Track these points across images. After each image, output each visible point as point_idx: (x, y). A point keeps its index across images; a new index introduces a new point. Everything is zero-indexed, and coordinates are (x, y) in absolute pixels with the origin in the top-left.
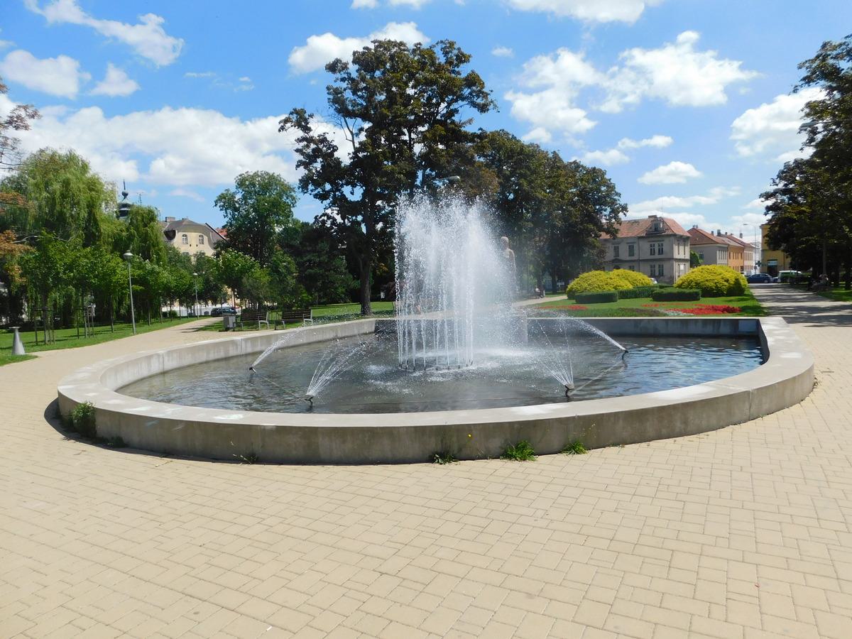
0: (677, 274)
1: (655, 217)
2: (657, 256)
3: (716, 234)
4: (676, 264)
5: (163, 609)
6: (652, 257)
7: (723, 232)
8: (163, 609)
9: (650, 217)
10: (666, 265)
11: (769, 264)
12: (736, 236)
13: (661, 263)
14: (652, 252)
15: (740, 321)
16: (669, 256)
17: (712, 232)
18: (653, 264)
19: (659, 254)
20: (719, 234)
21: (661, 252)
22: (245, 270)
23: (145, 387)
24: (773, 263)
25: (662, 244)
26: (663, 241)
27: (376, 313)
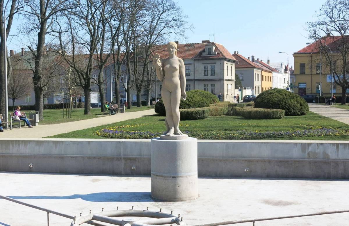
0: (226, 93)
1: (208, 42)
2: (210, 77)
3: (251, 60)
4: (225, 83)
5: (79, 225)
6: (206, 77)
7: (256, 59)
8: (79, 225)
9: (203, 42)
10: (217, 85)
11: (300, 87)
12: (265, 62)
13: (213, 83)
14: (206, 73)
15: (9, 105)
16: (219, 77)
17: (249, 58)
18: (206, 83)
19: (212, 75)
20: (253, 60)
21: (213, 74)
22: (22, 78)
23: (252, 66)
24: (302, 86)
25: (214, 66)
26: (215, 63)
27: (74, 157)
